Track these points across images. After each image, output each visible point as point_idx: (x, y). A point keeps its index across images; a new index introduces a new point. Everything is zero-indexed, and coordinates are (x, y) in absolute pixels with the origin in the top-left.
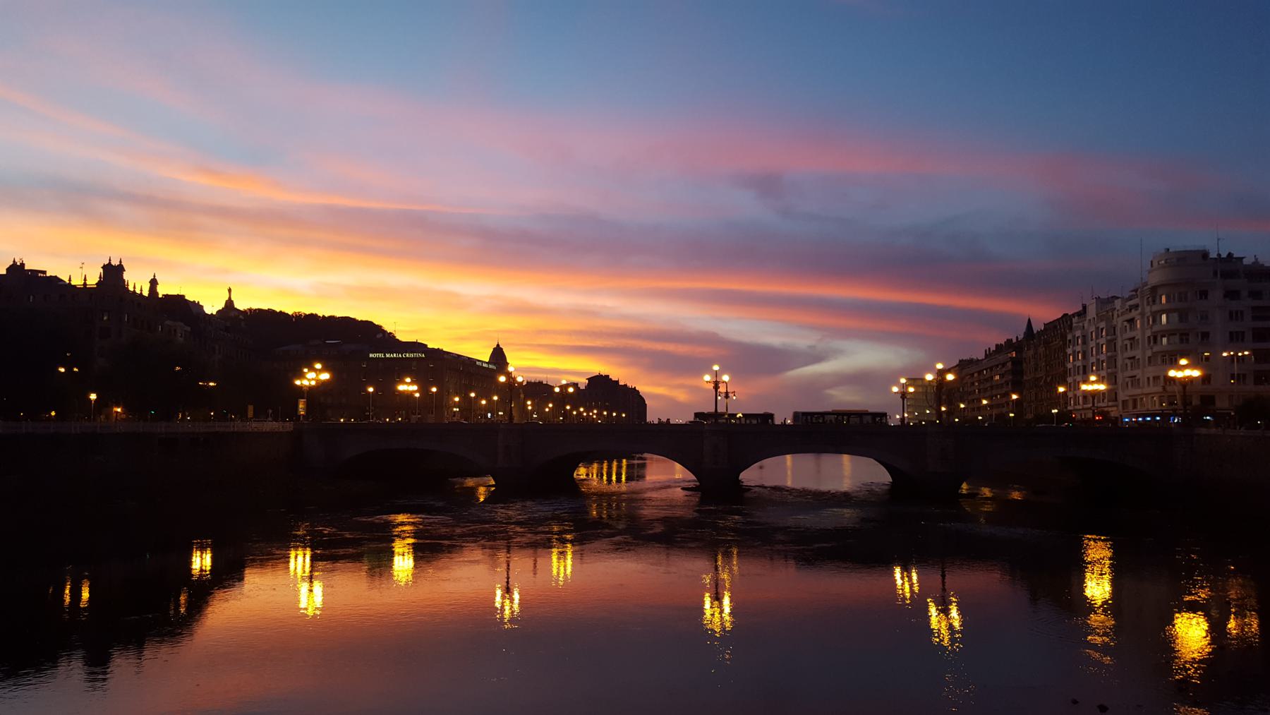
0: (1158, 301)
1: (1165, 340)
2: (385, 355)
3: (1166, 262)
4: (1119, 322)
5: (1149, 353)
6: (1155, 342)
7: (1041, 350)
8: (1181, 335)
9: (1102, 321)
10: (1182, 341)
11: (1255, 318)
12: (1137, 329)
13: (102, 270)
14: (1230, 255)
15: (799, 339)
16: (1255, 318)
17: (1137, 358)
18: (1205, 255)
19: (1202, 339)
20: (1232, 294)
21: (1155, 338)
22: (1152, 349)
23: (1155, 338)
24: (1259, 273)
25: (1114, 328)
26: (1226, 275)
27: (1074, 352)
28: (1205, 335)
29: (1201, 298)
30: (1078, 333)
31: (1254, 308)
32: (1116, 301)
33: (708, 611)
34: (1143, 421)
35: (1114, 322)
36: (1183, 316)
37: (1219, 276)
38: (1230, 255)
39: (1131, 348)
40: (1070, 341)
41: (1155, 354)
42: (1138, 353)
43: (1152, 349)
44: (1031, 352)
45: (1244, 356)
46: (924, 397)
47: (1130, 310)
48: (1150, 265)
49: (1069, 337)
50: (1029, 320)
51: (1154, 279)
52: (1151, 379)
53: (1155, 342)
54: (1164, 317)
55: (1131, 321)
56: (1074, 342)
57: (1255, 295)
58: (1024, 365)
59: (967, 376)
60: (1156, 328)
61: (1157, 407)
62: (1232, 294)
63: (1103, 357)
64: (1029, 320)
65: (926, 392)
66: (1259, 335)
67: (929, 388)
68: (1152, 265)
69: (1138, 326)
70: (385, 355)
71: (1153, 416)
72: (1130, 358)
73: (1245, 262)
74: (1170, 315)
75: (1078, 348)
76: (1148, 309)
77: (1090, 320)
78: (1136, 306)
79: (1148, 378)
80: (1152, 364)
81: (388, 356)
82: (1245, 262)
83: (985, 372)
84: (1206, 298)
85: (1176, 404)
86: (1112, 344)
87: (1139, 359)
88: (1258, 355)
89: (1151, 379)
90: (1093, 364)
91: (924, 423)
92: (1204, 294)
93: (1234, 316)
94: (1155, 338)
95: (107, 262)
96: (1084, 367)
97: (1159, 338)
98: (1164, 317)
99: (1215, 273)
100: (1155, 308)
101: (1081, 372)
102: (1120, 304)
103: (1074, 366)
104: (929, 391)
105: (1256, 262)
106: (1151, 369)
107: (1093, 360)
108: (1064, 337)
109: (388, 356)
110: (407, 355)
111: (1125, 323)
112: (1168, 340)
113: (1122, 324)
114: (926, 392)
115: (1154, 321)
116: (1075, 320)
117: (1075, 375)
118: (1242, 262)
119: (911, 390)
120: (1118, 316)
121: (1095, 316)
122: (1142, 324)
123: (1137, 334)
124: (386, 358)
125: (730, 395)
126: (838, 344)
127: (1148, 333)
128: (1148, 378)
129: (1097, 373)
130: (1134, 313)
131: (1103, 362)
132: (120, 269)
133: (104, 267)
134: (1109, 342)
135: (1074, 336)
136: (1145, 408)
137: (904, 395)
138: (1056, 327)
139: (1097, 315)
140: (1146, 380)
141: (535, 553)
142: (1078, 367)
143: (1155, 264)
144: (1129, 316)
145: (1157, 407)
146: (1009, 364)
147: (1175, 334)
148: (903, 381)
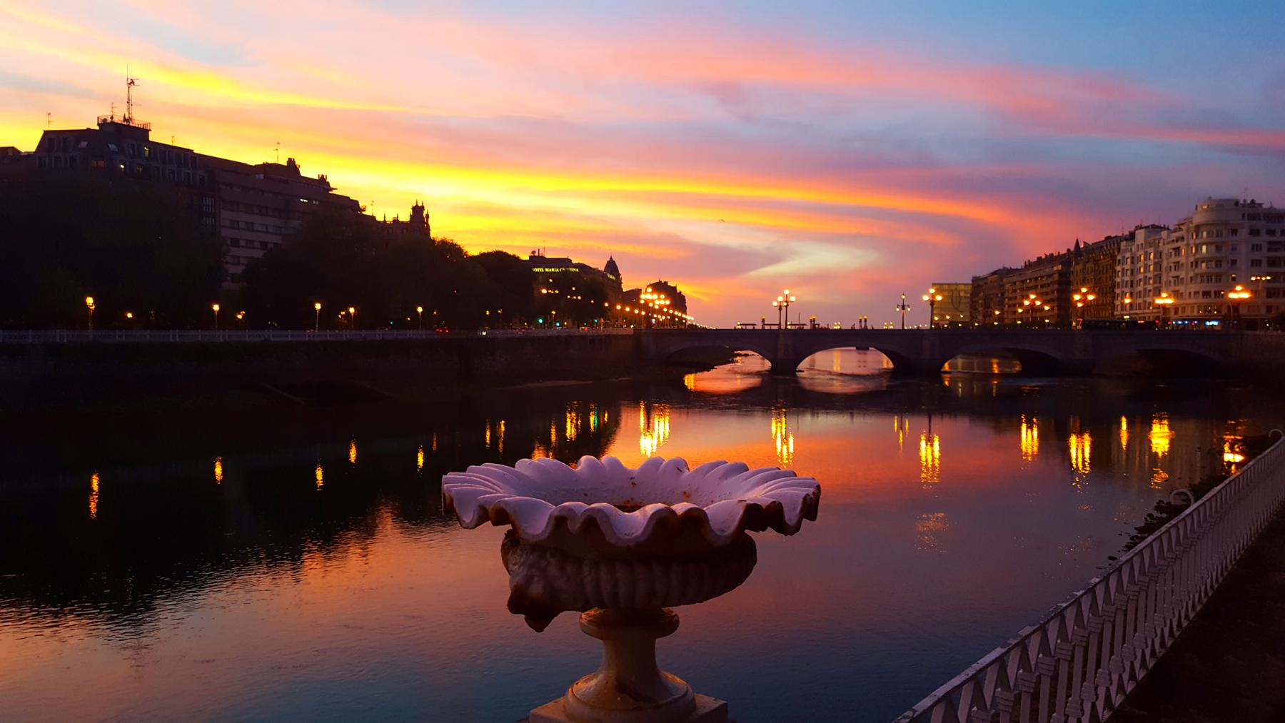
0: (1200, 236)
1: (1204, 265)
2: (544, 270)
3: (1208, 207)
4: (1166, 249)
5: (1191, 274)
6: (1196, 266)
7: (1090, 265)
8: (1217, 261)
9: (1151, 247)
10: (1216, 266)
11: (1269, 250)
12: (1182, 256)
13: (411, 211)
14: (1253, 201)
15: (759, 242)
16: (1269, 250)
17: (1181, 277)
18: (1237, 203)
19: (1232, 265)
20: (1255, 232)
21: (1197, 263)
22: (1194, 271)
23: (1196, 264)
24: (1275, 216)
25: (1161, 253)
26: (1253, 217)
27: (1123, 269)
28: (1234, 262)
29: (1232, 235)
30: (1128, 255)
31: (1269, 243)
32: (1162, 233)
33: (923, 453)
34: (621, 309)
35: (1161, 249)
36: (1218, 248)
37: (1246, 218)
38: (1253, 201)
39: (1175, 269)
40: (1119, 261)
41: (1196, 275)
42: (1182, 274)
43: (1194, 271)
44: (1079, 267)
45: (1266, 277)
46: (950, 301)
47: (1177, 241)
48: (1194, 208)
49: (1119, 257)
50: (1077, 240)
51: (1198, 219)
52: (1192, 294)
53: (1196, 266)
54: (1204, 248)
55: (1177, 250)
56: (1124, 261)
57: (1271, 232)
58: (1072, 277)
59: (1008, 283)
60: (1198, 256)
61: (1196, 313)
62: (1255, 232)
63: (1149, 275)
64: (1077, 240)
65: (952, 296)
66: (1273, 262)
67: (955, 293)
68: (1196, 208)
69: (1183, 253)
70: (544, 270)
71: (1183, 320)
72: (1174, 277)
73: (1264, 206)
74: (1209, 246)
75: (1128, 266)
76: (1192, 242)
77: (1138, 245)
78: (1182, 238)
79: (1190, 293)
80: (1193, 282)
81: (547, 270)
82: (1264, 206)
83: (1028, 281)
84: (1236, 234)
85: (1149, 308)
86: (1158, 266)
87: (1182, 278)
88: (1275, 277)
89: (1192, 294)
90: (1140, 280)
91: (960, 325)
92: (1234, 232)
93: (1256, 248)
94: (1197, 263)
95: (415, 205)
96: (1132, 282)
97: (1199, 263)
98: (1204, 248)
99: (1244, 216)
100: (1197, 241)
101: (1129, 285)
102: (1166, 235)
103: (1123, 281)
104: (954, 295)
105: (1271, 208)
106: (1193, 286)
107: (1141, 276)
108: (1113, 257)
109: (547, 270)
110: (558, 270)
111: (1171, 251)
112: (1207, 265)
113: (1168, 250)
114: (952, 296)
115: (1197, 250)
116: (1123, 244)
117: (1123, 287)
118: (1261, 207)
119: (939, 298)
120: (1164, 244)
121: (1143, 242)
122: (1187, 253)
123: (1182, 259)
124: (545, 272)
125: (906, 307)
126: (794, 245)
127: (1192, 259)
128: (1190, 293)
129: (1167, 291)
130: (1180, 244)
131: (1150, 278)
132: (422, 208)
133: (414, 208)
134: (1155, 264)
135: (1124, 257)
136: (1186, 314)
137: (932, 303)
138: (1102, 247)
139: (1145, 241)
140: (1188, 294)
141: (798, 416)
142: (1127, 282)
143: (1199, 209)
144: (1176, 245)
145: (1196, 313)
146: (1056, 276)
147: (1212, 261)
148: (932, 291)
